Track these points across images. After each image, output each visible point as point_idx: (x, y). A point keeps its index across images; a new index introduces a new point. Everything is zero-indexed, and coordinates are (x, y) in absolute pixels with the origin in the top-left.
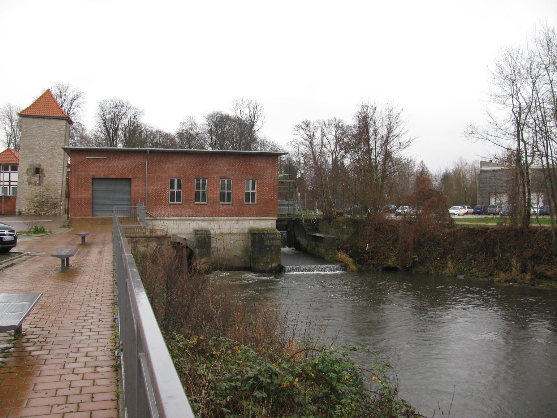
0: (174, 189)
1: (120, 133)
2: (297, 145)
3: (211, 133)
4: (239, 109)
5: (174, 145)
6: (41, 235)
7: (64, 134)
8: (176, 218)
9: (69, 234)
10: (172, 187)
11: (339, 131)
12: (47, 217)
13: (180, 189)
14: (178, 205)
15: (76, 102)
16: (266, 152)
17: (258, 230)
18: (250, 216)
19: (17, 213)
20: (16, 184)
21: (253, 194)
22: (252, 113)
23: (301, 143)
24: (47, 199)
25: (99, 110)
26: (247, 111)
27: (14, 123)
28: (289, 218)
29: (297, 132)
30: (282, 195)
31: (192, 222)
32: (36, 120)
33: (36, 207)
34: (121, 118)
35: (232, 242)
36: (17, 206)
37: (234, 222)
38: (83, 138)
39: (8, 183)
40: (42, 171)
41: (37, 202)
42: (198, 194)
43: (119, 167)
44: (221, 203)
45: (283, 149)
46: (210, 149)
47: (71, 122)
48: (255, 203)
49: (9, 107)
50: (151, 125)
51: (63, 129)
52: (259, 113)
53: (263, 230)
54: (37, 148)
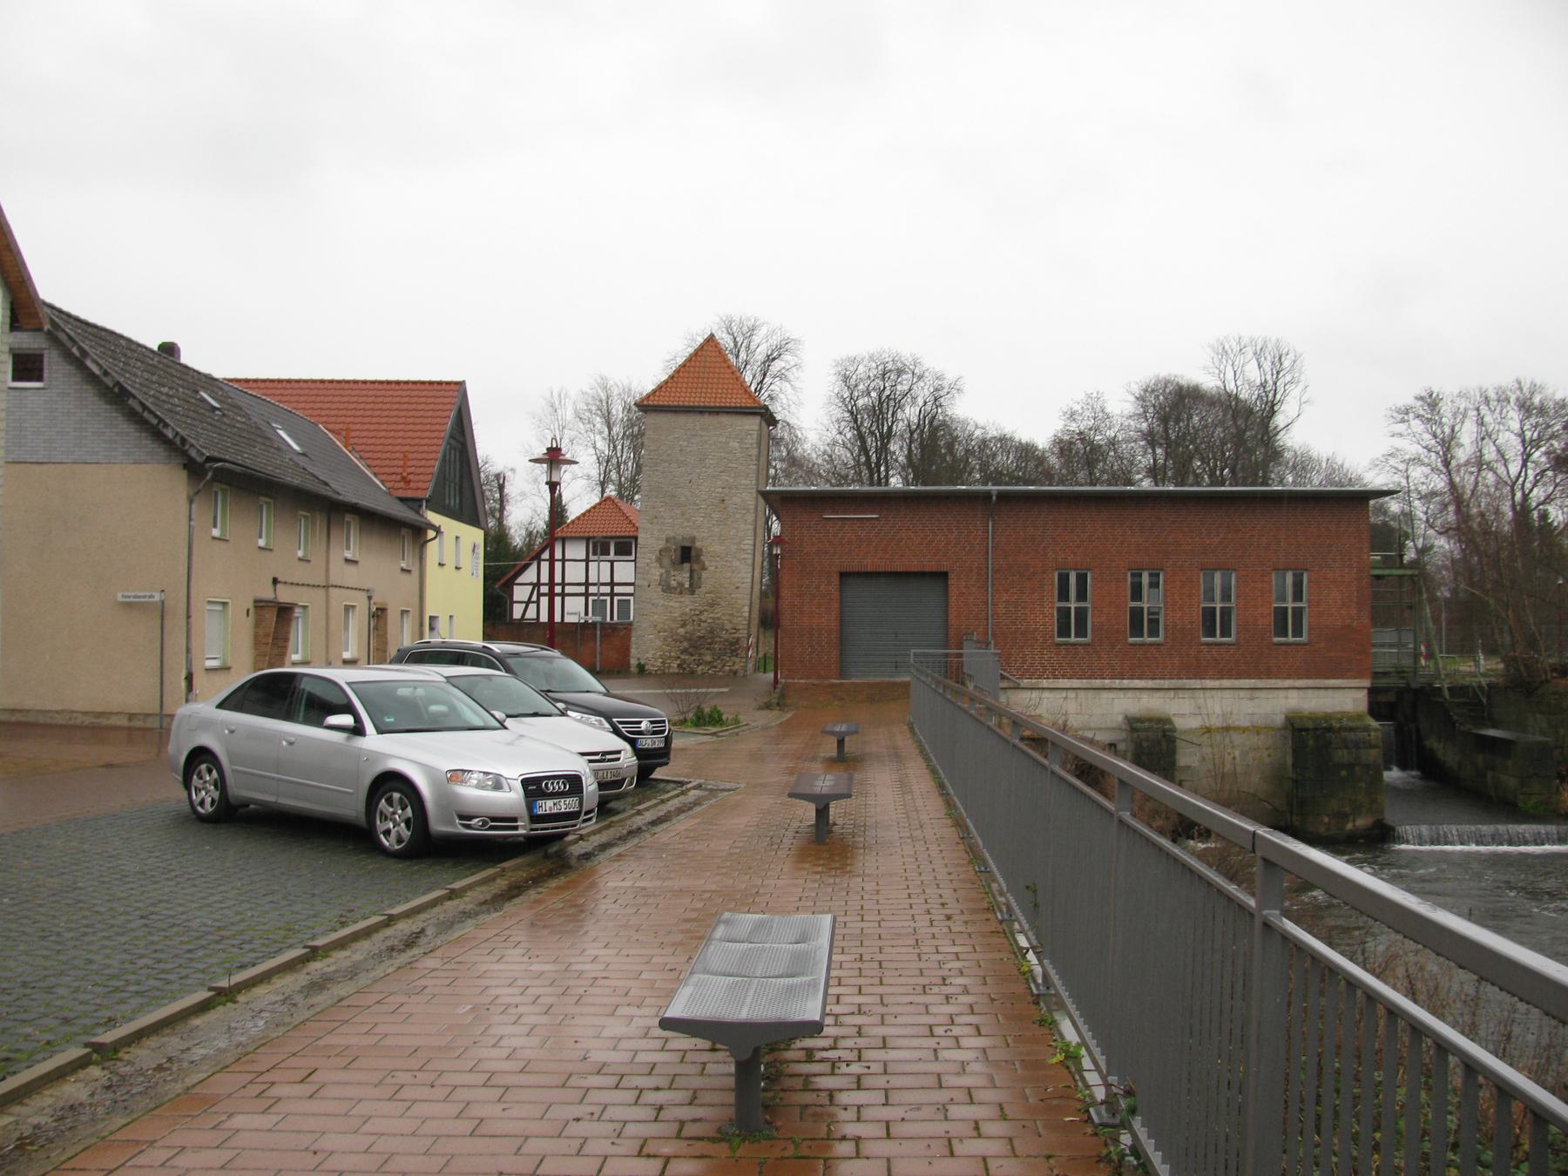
0: (1067, 600)
1: (894, 447)
2: (1402, 467)
3: (1151, 439)
4: (1229, 368)
5: (1048, 476)
6: (714, 730)
7: (754, 452)
8: (1076, 683)
9: (786, 729)
10: (1064, 595)
11: (1533, 420)
12: (713, 680)
13: (1085, 599)
14: (1082, 646)
15: (776, 366)
16: (1309, 488)
17: (1313, 717)
18: (1289, 677)
19: (634, 669)
20: (630, 589)
21: (1298, 613)
22: (1269, 377)
23: (1416, 460)
24: (711, 632)
25: (838, 386)
26: (1253, 373)
27: (615, 430)
28: (1401, 683)
29: (1401, 428)
30: (1381, 617)
31: (1121, 694)
32: (682, 419)
33: (683, 652)
34: (899, 406)
35: (1237, 753)
36: (633, 651)
37: (1242, 694)
38: (793, 461)
39: (607, 589)
41: (689, 640)
42: (1136, 615)
43: (915, 544)
44: (1205, 639)
45: (1359, 478)
46: (1146, 485)
47: (769, 419)
48: (1304, 639)
49: (605, 388)
50: (981, 423)
51: (752, 440)
52: (1288, 378)
53: (1328, 717)
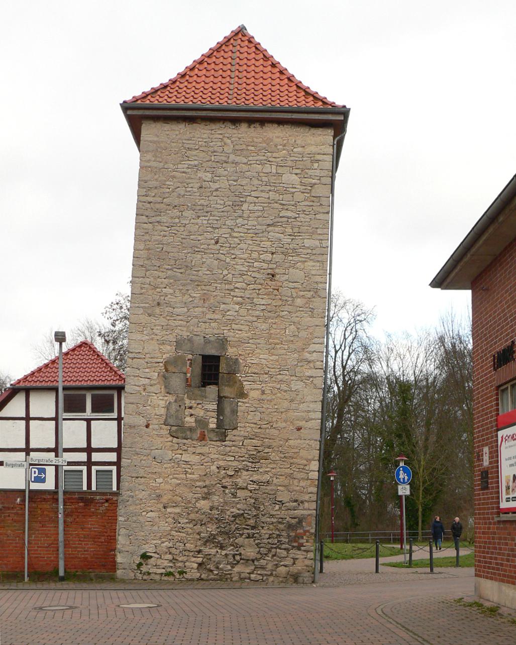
31: (44, 591)
32: (201, 133)
39: (83, 457)
40: (232, 373)
54: (209, 260)
